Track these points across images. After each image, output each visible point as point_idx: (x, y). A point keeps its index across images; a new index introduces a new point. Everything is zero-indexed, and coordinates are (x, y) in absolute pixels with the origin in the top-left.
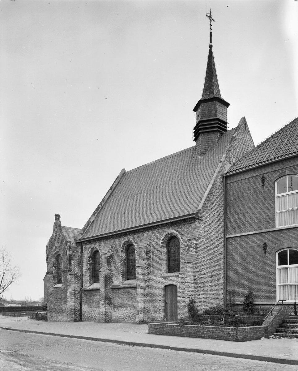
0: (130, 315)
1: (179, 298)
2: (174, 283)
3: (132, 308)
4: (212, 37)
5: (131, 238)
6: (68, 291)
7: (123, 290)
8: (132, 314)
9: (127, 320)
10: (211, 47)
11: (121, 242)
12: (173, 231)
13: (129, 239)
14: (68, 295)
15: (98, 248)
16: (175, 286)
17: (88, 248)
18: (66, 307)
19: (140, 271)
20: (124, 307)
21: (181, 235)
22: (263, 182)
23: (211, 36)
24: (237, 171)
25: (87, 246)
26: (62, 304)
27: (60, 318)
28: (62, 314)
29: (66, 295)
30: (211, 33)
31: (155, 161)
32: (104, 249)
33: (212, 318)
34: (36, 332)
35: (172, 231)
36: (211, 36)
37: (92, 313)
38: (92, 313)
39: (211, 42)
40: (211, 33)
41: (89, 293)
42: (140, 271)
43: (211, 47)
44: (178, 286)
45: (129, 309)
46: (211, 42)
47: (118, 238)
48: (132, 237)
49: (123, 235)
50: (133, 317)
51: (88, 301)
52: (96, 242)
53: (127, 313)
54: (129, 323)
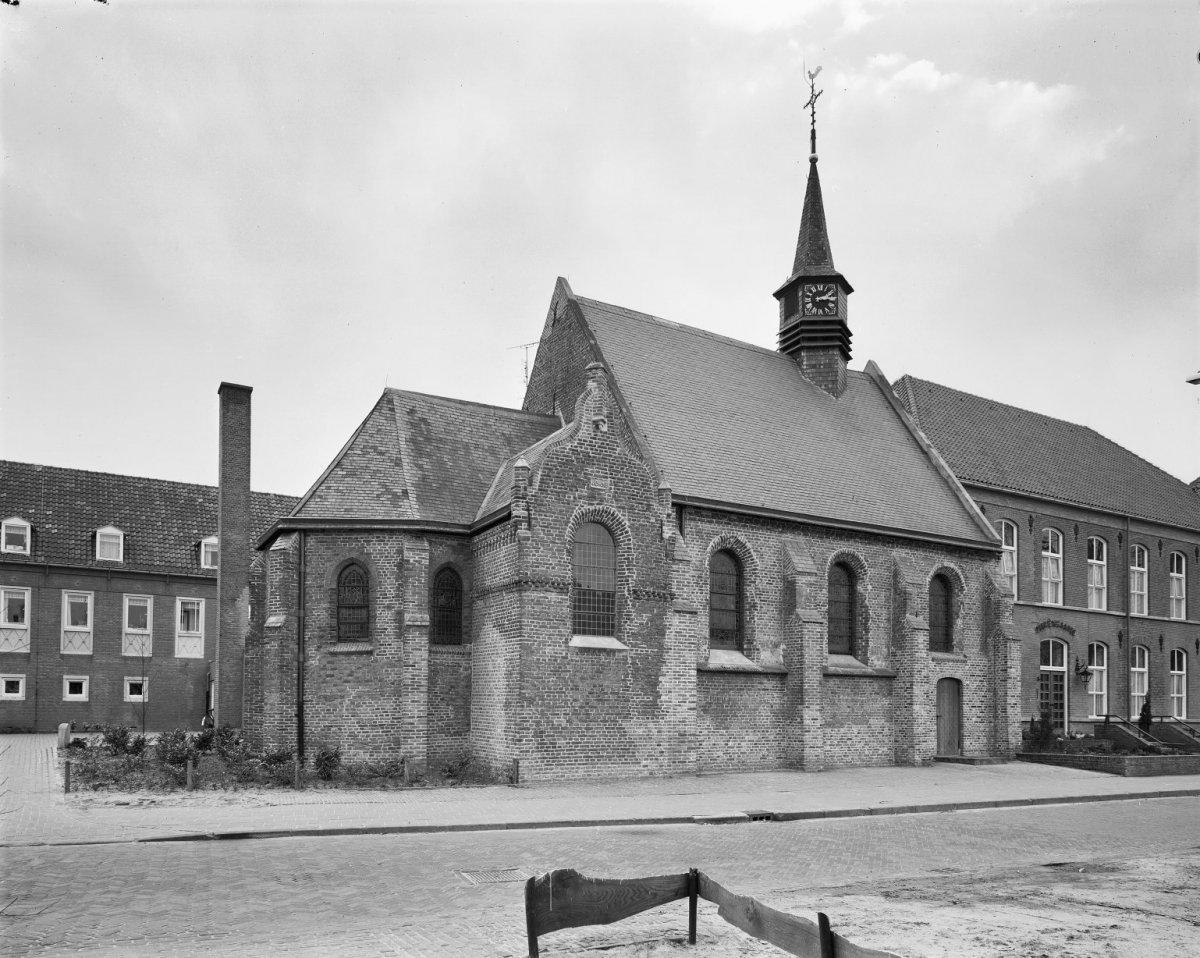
0: (859, 746)
1: (966, 708)
2: (957, 676)
3: (863, 728)
4: (817, 141)
5: (860, 550)
6: (664, 669)
7: (837, 681)
8: (862, 744)
9: (849, 759)
10: (813, 161)
11: (719, 533)
12: (952, 565)
13: (851, 550)
14: (665, 682)
15: (749, 545)
16: (958, 682)
17: (710, 536)
18: (651, 725)
19: (921, 640)
20: (842, 725)
21: (966, 578)
22: (1160, 549)
23: (813, 137)
24: (1032, 495)
25: (706, 527)
26: (627, 717)
27: (616, 769)
28: (626, 751)
29: (655, 684)
30: (813, 132)
31: (683, 327)
32: (762, 550)
33: (1061, 743)
34: (996, 804)
35: (950, 563)
36: (813, 137)
37: (730, 744)
38: (730, 744)
39: (814, 151)
40: (813, 132)
41: (720, 681)
42: (921, 640)
43: (813, 161)
44: (966, 682)
45: (855, 731)
46: (814, 151)
47: (822, 538)
48: (861, 546)
49: (757, 523)
50: (867, 752)
51: (714, 706)
52: (744, 526)
53: (849, 742)
54: (854, 766)
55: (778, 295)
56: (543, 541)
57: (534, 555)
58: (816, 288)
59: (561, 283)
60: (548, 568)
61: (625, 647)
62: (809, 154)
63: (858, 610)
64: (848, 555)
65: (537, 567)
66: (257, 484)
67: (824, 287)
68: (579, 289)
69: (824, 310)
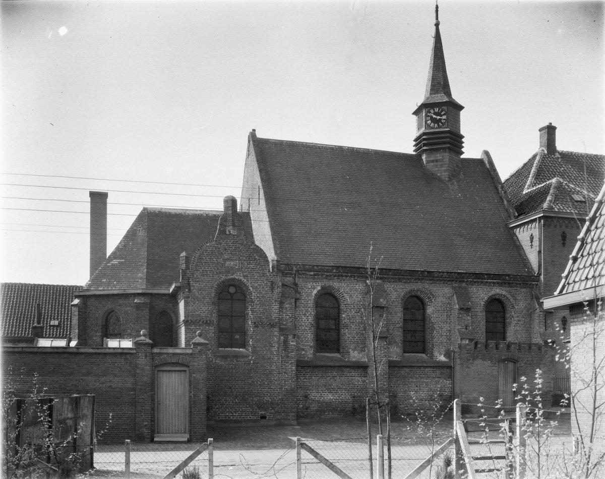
4: (439, 12)
10: (437, 25)
23: (437, 11)
35: (497, 291)
36: (437, 11)
43: (437, 25)
55: (417, 113)
56: (197, 298)
57: (192, 306)
58: (434, 110)
59: (254, 130)
60: (201, 312)
61: (206, 342)
62: (434, 21)
63: (427, 326)
64: (505, 296)
65: (195, 312)
66: (124, 453)
67: (439, 110)
68: (259, 135)
69: (438, 125)
